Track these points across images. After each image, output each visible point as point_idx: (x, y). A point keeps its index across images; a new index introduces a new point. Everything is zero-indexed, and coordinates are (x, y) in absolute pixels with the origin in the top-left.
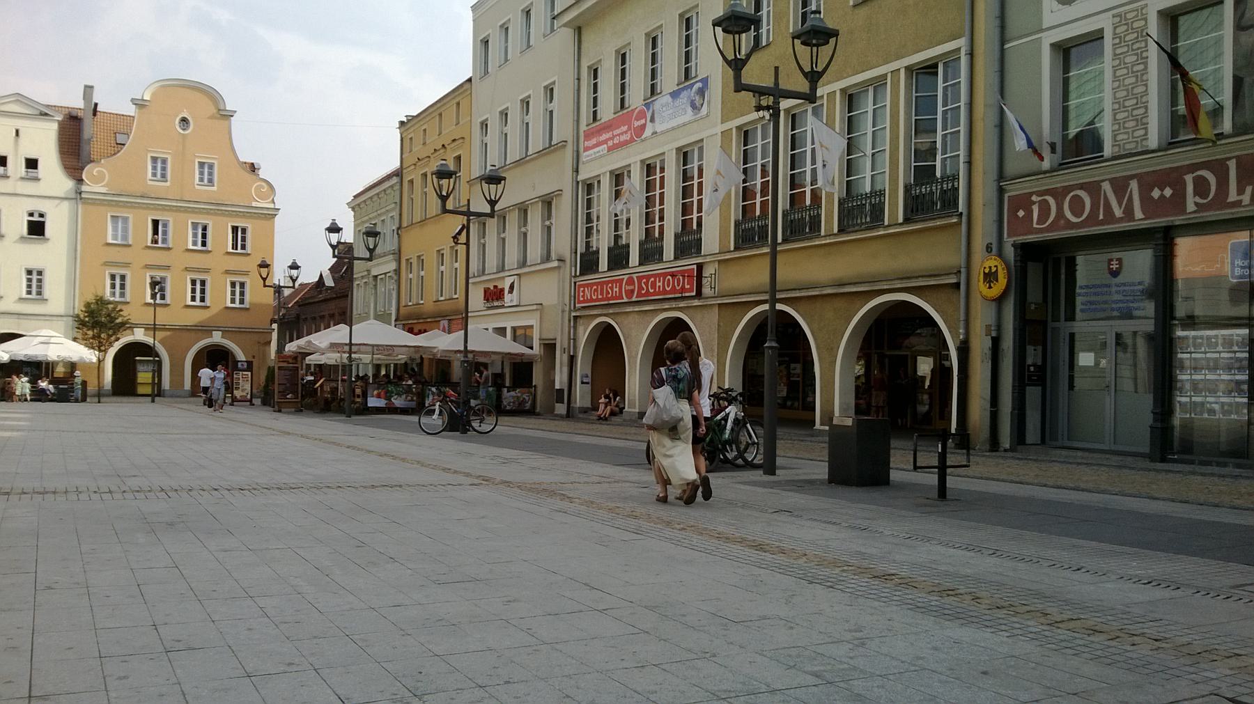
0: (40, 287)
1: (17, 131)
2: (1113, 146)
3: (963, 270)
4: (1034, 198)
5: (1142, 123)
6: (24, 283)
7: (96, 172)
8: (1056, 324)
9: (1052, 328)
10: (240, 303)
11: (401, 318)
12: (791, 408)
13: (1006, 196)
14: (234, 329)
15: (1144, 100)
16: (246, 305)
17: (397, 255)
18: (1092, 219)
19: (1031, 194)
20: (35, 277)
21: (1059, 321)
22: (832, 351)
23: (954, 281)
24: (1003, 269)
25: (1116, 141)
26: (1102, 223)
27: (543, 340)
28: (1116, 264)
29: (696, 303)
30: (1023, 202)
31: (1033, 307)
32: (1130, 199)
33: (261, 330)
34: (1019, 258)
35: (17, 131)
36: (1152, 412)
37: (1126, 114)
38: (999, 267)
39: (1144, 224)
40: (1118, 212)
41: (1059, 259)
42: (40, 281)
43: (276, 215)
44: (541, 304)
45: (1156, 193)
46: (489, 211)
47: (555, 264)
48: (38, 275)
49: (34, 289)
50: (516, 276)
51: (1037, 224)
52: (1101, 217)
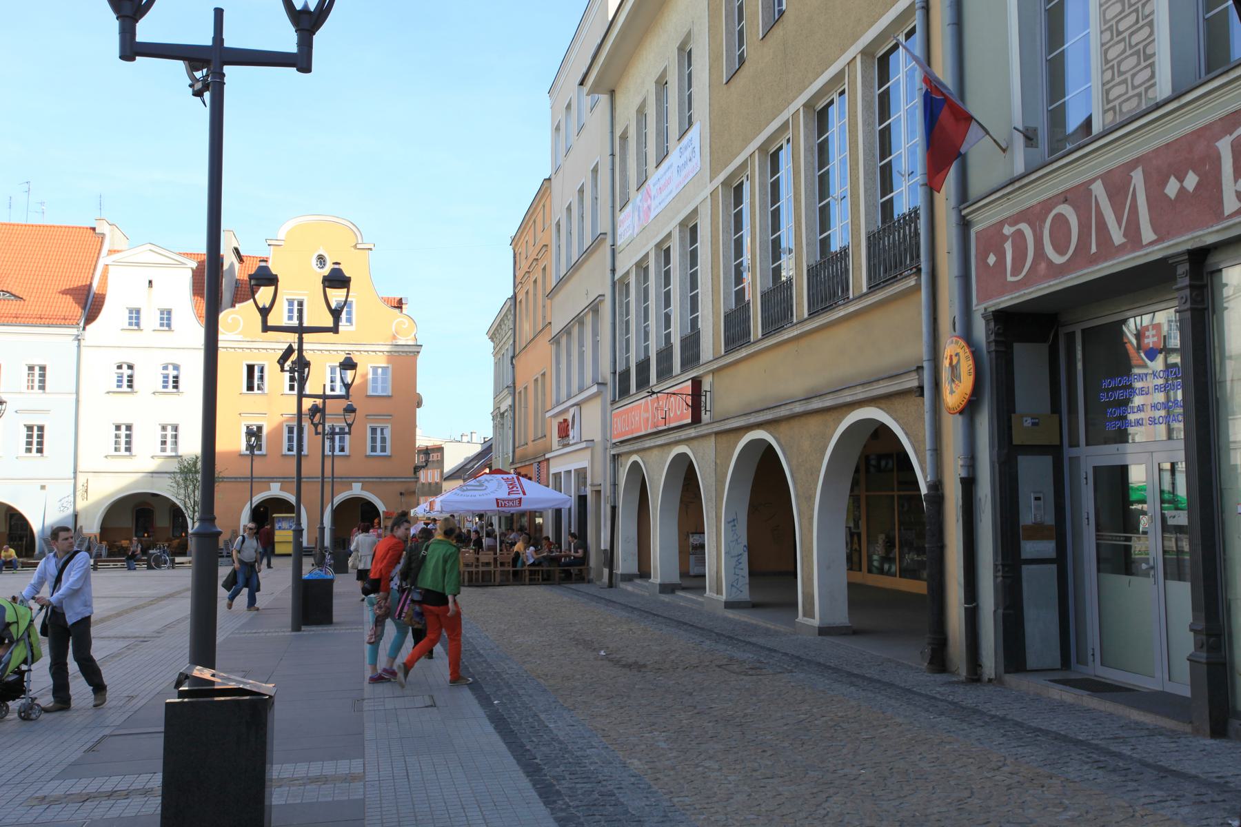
0: (128, 443)
1: (150, 282)
2: (1105, 112)
3: (925, 364)
4: (1008, 230)
5: (1146, 57)
6: (24, 440)
7: (232, 319)
8: (1074, 452)
9: (1070, 458)
10: (381, 451)
11: (516, 461)
12: (889, 573)
13: (973, 232)
14: (374, 480)
15: (1147, 11)
16: (388, 452)
17: (512, 389)
18: (1082, 256)
19: (1001, 224)
20: (123, 432)
21: (1078, 446)
22: (810, 499)
23: (915, 384)
24: (967, 357)
25: (1108, 102)
26: (1094, 260)
27: (595, 486)
28: (1153, 336)
29: (692, 432)
30: (994, 240)
31: (1028, 422)
32: (1134, 207)
33: (403, 480)
34: (992, 337)
35: (150, 282)
36: (1191, 630)
37: (1121, 46)
38: (962, 355)
39: (1153, 252)
40: (1117, 237)
41: (1074, 333)
42: (128, 436)
43: (418, 352)
44: (593, 440)
45: (1172, 188)
46: (331, 325)
47: (595, 389)
48: (127, 430)
49: (123, 446)
50: (575, 407)
51: (1013, 275)
52: (1094, 249)
